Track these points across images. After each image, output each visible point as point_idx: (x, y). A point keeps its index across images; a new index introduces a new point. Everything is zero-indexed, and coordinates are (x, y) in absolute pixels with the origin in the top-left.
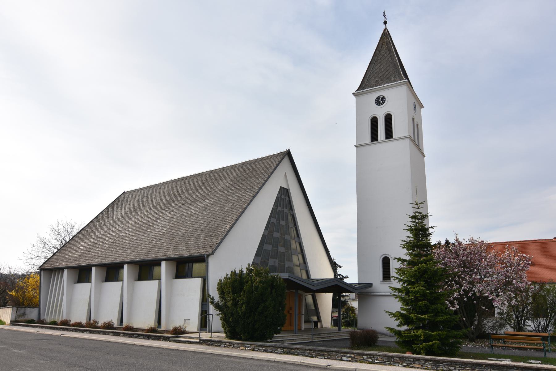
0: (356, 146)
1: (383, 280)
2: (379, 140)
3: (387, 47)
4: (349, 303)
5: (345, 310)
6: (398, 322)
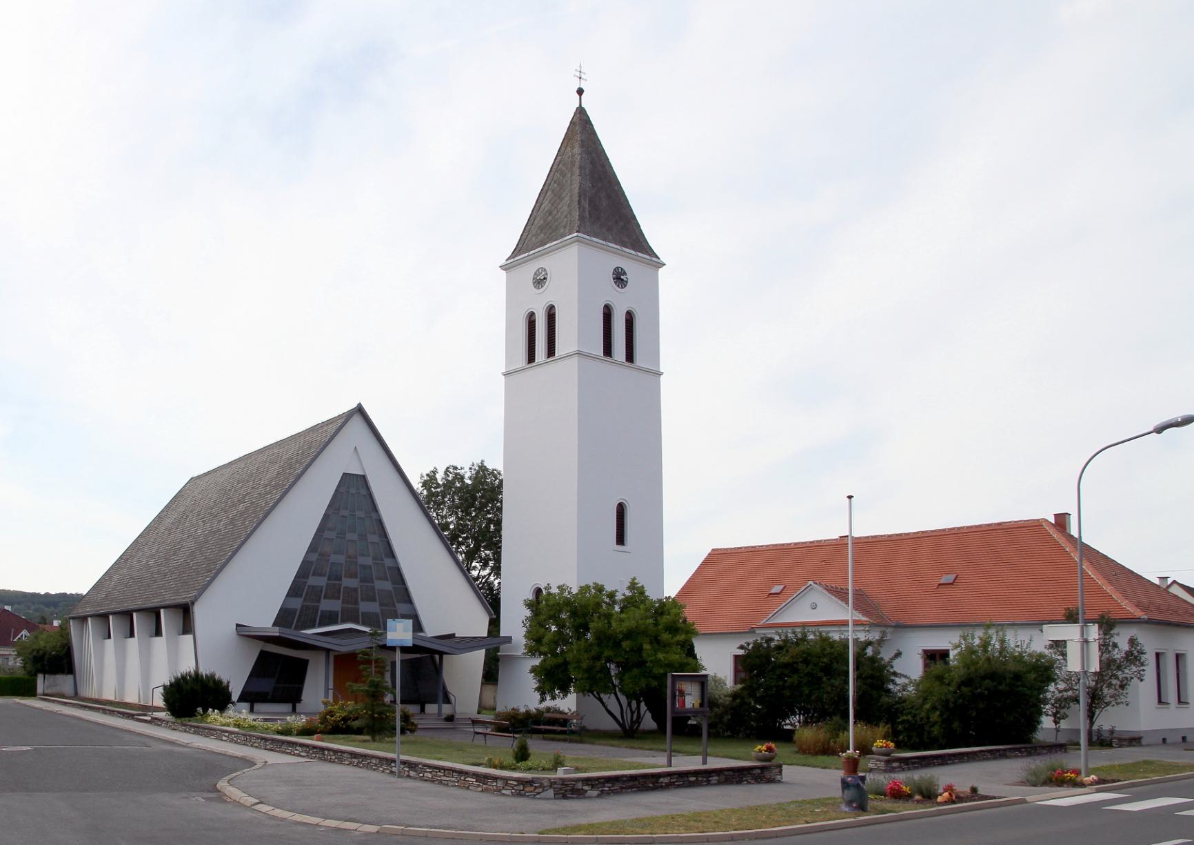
0: (505, 375)
2: (536, 361)
6: (1061, 727)
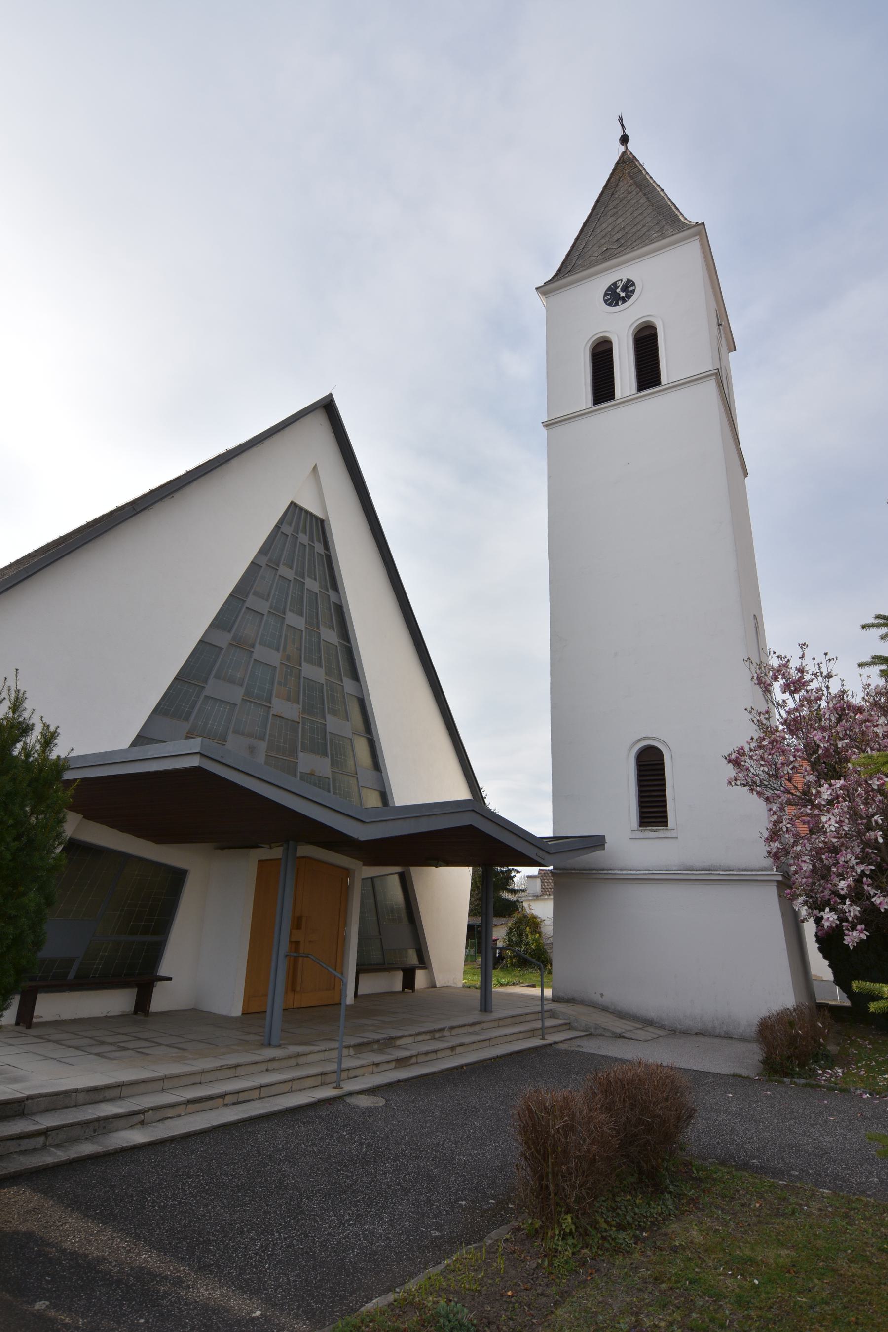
0: (548, 425)
1: (640, 826)
3: (631, 181)
4: (525, 904)
5: (515, 924)
